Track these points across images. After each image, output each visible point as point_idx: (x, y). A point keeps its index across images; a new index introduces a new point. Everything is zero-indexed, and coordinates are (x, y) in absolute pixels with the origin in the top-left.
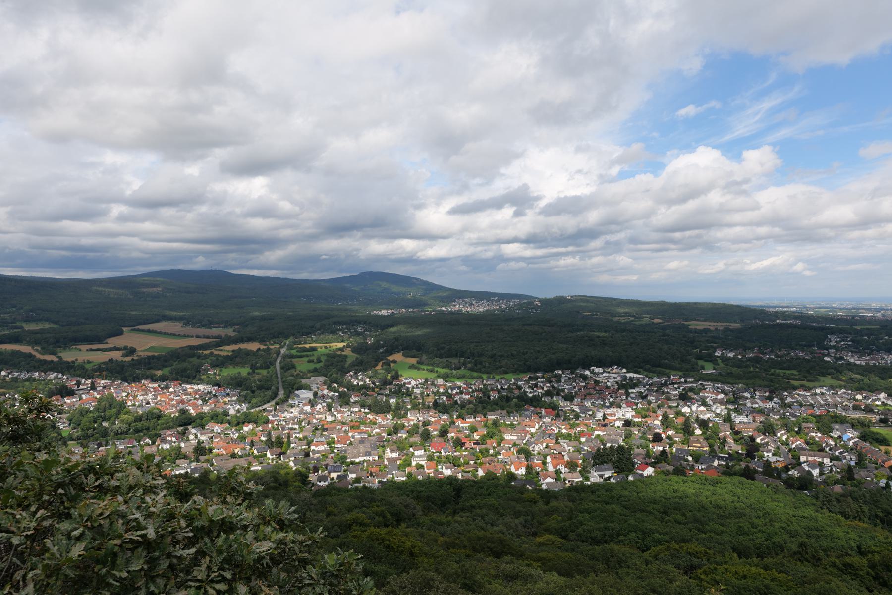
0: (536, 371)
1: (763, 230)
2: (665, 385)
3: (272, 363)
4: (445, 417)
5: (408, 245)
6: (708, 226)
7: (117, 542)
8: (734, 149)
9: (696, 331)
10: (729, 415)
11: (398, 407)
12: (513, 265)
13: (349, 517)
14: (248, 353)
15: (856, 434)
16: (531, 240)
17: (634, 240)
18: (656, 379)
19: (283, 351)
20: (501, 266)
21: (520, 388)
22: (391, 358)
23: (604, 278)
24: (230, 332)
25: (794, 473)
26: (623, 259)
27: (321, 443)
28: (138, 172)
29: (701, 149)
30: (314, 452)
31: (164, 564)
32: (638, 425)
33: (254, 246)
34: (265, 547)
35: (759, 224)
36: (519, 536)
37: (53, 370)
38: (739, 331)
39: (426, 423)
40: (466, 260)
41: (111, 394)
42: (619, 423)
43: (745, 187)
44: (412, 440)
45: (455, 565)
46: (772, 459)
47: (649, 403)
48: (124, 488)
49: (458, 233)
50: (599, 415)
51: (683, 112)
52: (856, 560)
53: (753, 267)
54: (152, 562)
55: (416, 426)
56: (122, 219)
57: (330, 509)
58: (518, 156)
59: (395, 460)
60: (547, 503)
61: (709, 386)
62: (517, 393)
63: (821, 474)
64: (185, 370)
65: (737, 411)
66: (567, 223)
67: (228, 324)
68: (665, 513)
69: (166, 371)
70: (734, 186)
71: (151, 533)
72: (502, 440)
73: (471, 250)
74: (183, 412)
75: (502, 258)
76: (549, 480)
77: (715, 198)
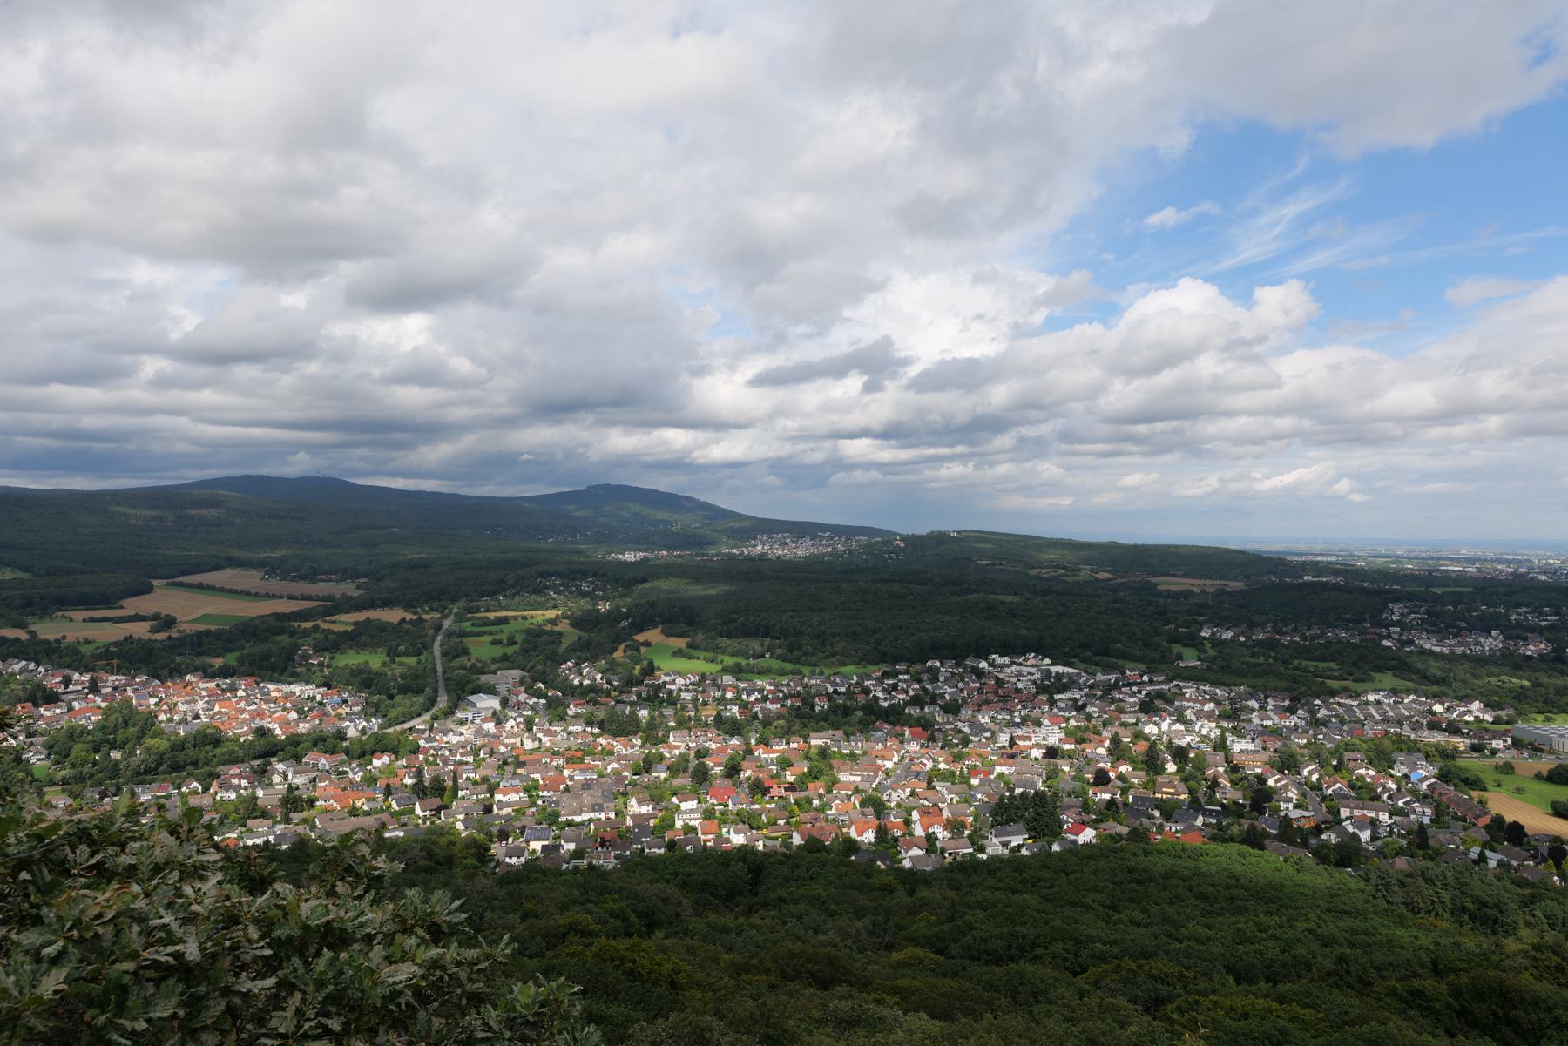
0: (896, 661)
1: (1284, 423)
2: (1116, 686)
3: (427, 646)
4: (735, 742)
5: (676, 439)
6: (1191, 414)
7: (129, 966)
8: (1239, 284)
9: (1170, 595)
10: (1223, 739)
11: (652, 725)
12: (858, 475)
13: (562, 920)
14: (383, 627)
15: (1433, 770)
16: (891, 433)
17: (1067, 437)
18: (1101, 677)
19: (447, 623)
20: (839, 476)
21: (866, 691)
22: (640, 638)
23: (1016, 502)
24: (350, 589)
25: (1330, 837)
26: (1049, 469)
27: (514, 789)
28: (194, 301)
29: (1185, 282)
30: (501, 805)
31: (217, 1007)
32: (1069, 755)
33: (399, 436)
34: (403, 973)
35: (1279, 412)
36: (862, 951)
37: (19, 655)
38: (1240, 594)
39: (701, 753)
40: (776, 465)
41: (128, 701)
42: (1036, 753)
43: (1257, 349)
44: (677, 782)
45: (750, 1004)
46: (1294, 814)
47: (1089, 717)
48: (145, 870)
49: (762, 419)
50: (1004, 739)
51: (1155, 219)
52: (1429, 984)
53: (1268, 485)
54: (194, 1004)
55: (684, 758)
56: (162, 382)
57: (528, 906)
58: (876, 287)
59: (647, 817)
60: (912, 892)
61: (1190, 690)
62: (861, 699)
63: (1374, 838)
64: (266, 657)
65: (1236, 731)
66: (956, 404)
67: (347, 574)
68: (1114, 908)
69: (231, 659)
70: (1240, 347)
71: (192, 951)
72: (835, 782)
73: (786, 449)
74: (262, 732)
75: (841, 464)
76: (916, 852)
77: (1207, 366)
